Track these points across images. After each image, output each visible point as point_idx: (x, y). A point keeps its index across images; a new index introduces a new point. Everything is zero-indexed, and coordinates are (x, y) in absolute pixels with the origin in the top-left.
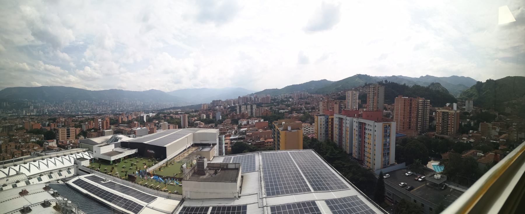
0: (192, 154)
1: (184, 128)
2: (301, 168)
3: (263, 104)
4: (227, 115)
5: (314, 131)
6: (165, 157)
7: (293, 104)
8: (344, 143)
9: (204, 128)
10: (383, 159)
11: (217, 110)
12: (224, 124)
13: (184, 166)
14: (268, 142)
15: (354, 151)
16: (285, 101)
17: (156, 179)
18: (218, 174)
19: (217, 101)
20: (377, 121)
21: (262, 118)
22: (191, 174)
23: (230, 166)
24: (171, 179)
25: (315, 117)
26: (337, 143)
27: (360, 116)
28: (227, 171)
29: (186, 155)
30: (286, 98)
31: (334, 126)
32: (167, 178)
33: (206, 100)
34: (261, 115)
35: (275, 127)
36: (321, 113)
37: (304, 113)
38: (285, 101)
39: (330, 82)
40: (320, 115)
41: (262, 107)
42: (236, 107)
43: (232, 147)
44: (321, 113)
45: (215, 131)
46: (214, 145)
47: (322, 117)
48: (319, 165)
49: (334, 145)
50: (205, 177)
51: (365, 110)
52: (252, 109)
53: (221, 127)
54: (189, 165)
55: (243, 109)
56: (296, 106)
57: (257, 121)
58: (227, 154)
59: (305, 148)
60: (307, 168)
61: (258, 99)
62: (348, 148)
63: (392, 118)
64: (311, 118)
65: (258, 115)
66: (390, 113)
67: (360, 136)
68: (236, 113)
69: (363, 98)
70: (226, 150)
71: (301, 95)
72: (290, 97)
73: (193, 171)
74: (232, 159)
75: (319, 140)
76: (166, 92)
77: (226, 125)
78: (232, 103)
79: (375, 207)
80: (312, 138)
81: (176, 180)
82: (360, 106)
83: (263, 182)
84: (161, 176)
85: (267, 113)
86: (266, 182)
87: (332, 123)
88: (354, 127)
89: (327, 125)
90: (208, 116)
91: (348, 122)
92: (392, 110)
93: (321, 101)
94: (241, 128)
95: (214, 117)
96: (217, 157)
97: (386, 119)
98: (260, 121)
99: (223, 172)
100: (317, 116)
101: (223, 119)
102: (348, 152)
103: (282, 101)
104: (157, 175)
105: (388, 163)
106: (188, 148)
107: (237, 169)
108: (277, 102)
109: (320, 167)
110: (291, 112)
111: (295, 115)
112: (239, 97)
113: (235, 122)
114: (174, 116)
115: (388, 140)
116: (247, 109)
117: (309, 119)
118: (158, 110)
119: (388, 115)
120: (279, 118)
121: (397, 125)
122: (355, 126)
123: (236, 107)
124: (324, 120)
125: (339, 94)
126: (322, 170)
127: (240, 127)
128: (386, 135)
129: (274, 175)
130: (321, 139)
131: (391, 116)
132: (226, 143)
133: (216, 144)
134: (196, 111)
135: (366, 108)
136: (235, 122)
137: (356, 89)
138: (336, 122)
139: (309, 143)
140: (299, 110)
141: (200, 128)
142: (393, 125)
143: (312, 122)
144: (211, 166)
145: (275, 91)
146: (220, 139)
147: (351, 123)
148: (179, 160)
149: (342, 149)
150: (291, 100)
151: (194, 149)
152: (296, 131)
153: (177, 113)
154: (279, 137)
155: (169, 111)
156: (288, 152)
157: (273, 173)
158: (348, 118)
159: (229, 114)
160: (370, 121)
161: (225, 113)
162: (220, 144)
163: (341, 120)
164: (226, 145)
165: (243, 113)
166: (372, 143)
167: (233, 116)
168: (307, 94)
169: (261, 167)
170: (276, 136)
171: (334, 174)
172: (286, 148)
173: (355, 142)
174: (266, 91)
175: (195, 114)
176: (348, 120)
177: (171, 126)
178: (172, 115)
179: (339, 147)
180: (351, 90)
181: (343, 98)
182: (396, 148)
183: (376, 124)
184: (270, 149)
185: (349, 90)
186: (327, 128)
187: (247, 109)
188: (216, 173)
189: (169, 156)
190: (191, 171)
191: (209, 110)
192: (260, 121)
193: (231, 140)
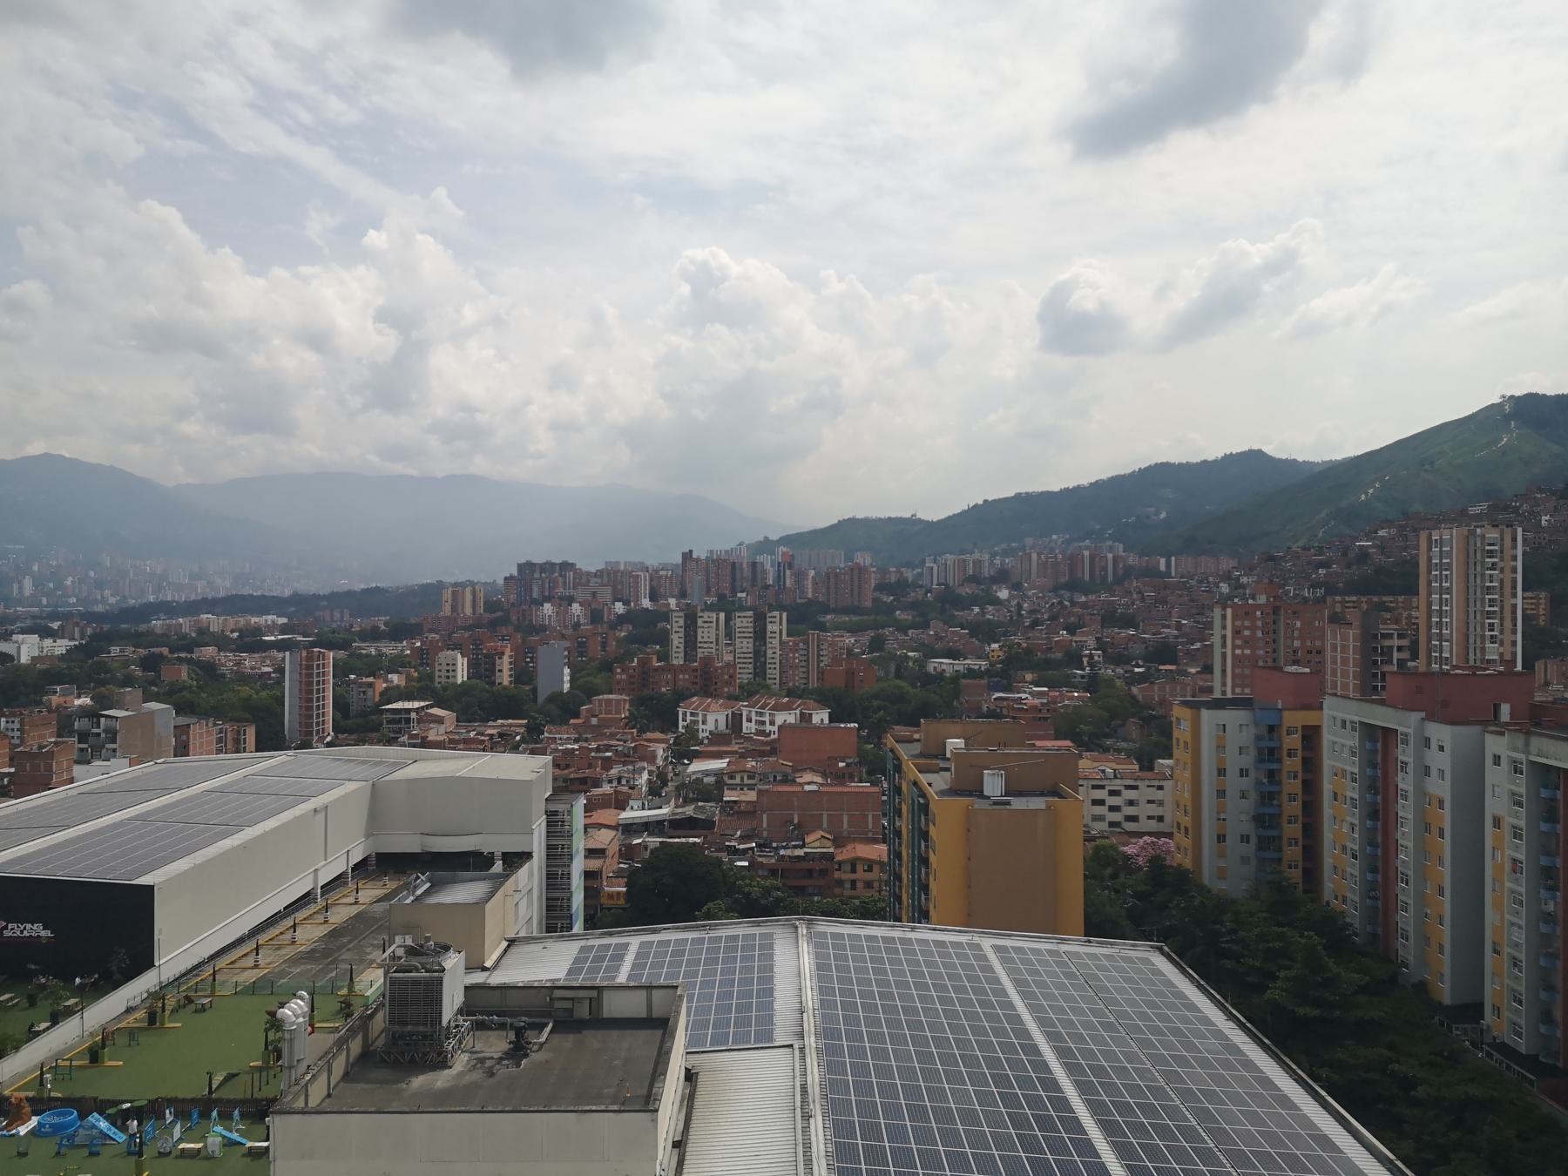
0: (360, 925)
1: (306, 745)
3: (826, 610)
4: (607, 667)
5: (1167, 811)
6: (143, 960)
7: (1016, 622)
8: (1406, 919)
9: (451, 744)
11: (543, 628)
12: (587, 726)
13: (294, 1011)
14: (853, 864)
15: (1491, 990)
16: (964, 603)
17: (57, 1129)
19: (548, 567)
21: (823, 700)
22: (339, 1066)
23: (615, 1006)
24: (179, 1115)
25: (1178, 712)
28: (592, 1038)
29: (310, 934)
30: (975, 579)
31: (1327, 788)
32: (150, 1111)
34: (814, 683)
35: (898, 768)
37: (1092, 684)
38: (964, 603)
39: (1291, 464)
40: (1220, 704)
41: (822, 627)
42: (665, 616)
43: (631, 877)
44: (1223, 684)
45: (526, 768)
46: (515, 860)
47: (1234, 718)
48: (1204, 1063)
49: (1331, 927)
50: (441, 1079)
52: (760, 635)
53: (564, 740)
54: (330, 1005)
55: (709, 630)
56: (1039, 636)
57: (790, 718)
58: (593, 922)
59: (1097, 927)
60: (1121, 1071)
61: (800, 576)
64: (1147, 721)
65: (797, 680)
68: (664, 656)
70: (591, 893)
71: (1074, 561)
72: (1002, 577)
73: (356, 1046)
74: (633, 955)
76: (175, 475)
77: (597, 731)
78: (644, 589)
80: (1157, 864)
81: (225, 1117)
83: (817, 1123)
84: (101, 1107)
85: (850, 674)
86: (840, 1129)
87: (1311, 763)
88: (1495, 804)
90: (483, 667)
91: (1439, 761)
93: (1224, 602)
98: (806, 718)
99: (568, 1041)
100: (1195, 706)
101: (584, 691)
102: (1445, 992)
103: (949, 601)
104: (68, 1102)
106: (328, 887)
107: (662, 1025)
108: (914, 605)
110: (1004, 675)
111: (1030, 695)
113: (656, 712)
114: (227, 661)
116: (729, 634)
117: (1133, 727)
118: (90, 617)
120: (926, 711)
124: (1247, 737)
125: (1364, 555)
126: (1236, 1099)
127: (684, 750)
129: (888, 1090)
130: (1222, 874)
132: (591, 853)
133: (528, 856)
134: (398, 632)
136: (656, 712)
138: (1340, 757)
139: (1134, 899)
141: (425, 744)
143: (1153, 743)
144: (488, 1007)
146: (556, 825)
148: (250, 977)
150: (1003, 594)
151: (370, 893)
152: (1038, 803)
153: (251, 642)
154: (925, 835)
155: (185, 623)
156: (987, 943)
157: (884, 1072)
158: (1440, 733)
159: (623, 659)
161: (596, 650)
162: (557, 855)
163: (1379, 741)
164: (595, 864)
165: (707, 661)
167: (645, 673)
168: (1113, 551)
169: (809, 1024)
170: (904, 825)
171: (1325, 1142)
174: (848, 531)
175: (389, 649)
176: (1435, 750)
177: (202, 732)
178: (209, 652)
180: (1460, 517)
181: (1400, 579)
184: (868, 912)
185: (1438, 521)
187: (729, 634)
188: (518, 1050)
189: (175, 953)
190: (341, 1043)
191: (493, 625)
192: (806, 718)
193: (629, 829)
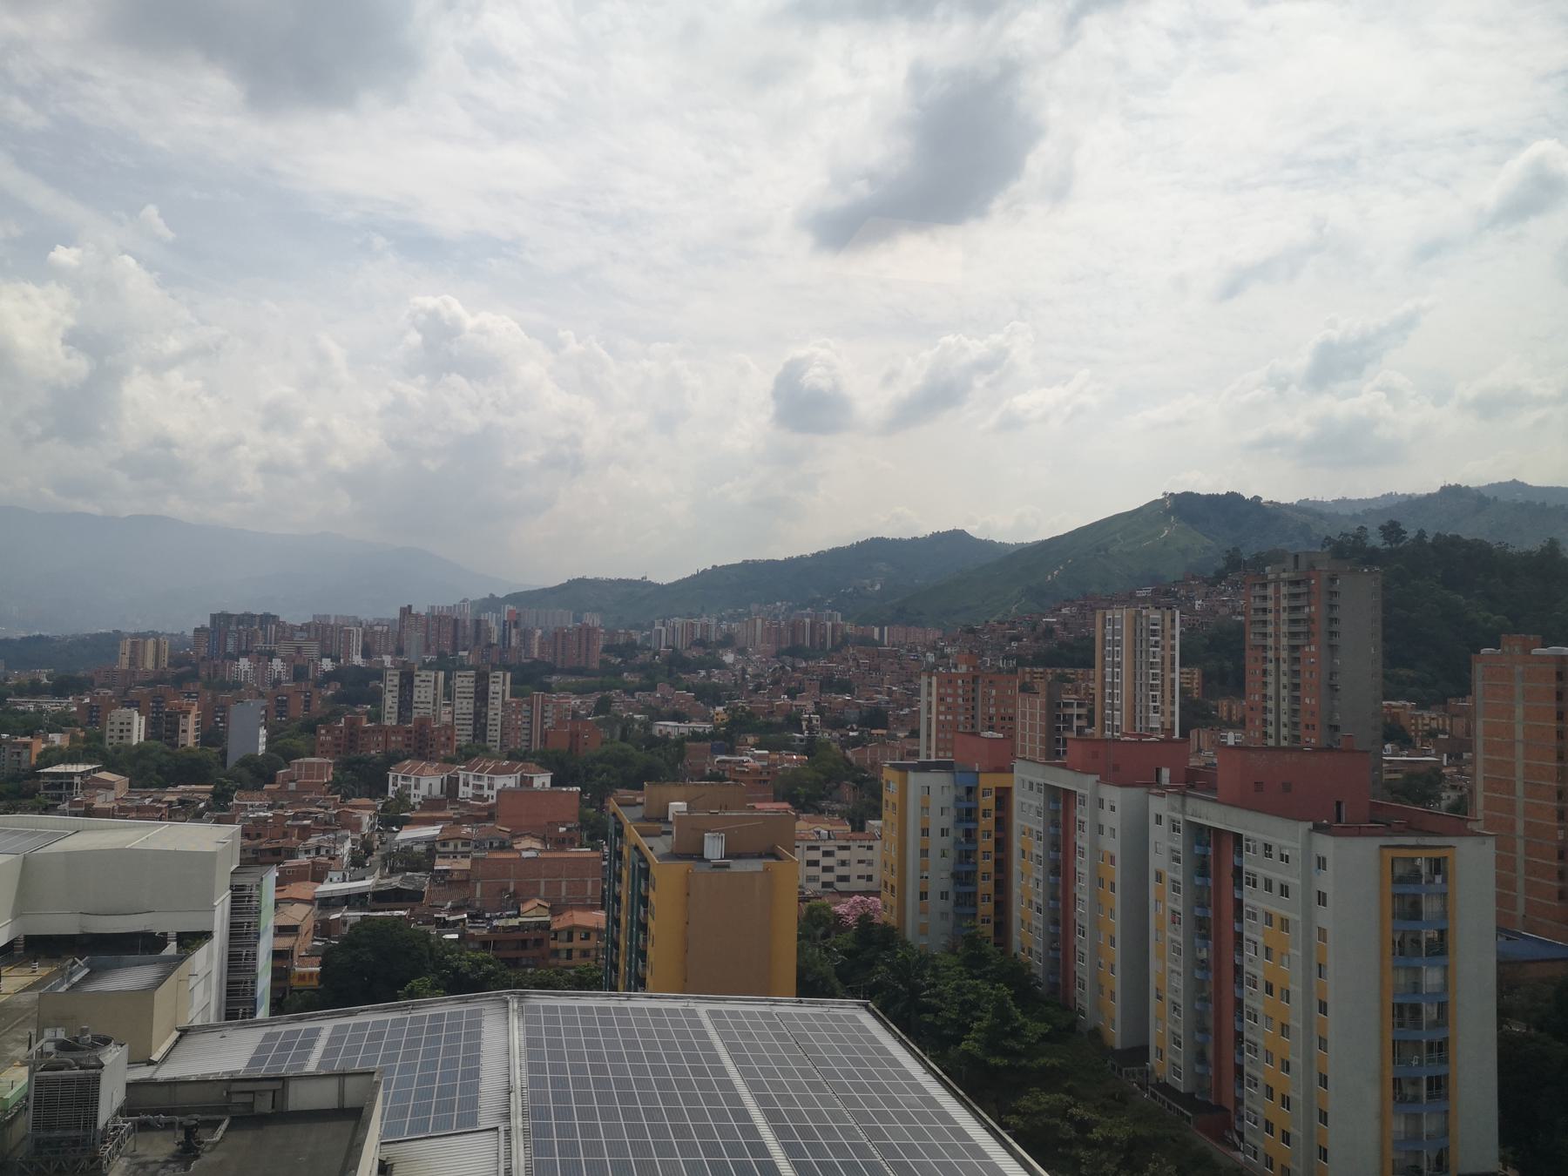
3: (553, 670)
4: (310, 728)
5: (877, 872)
8: (1082, 969)
9: (122, 812)
10: (1399, 1126)
11: (237, 685)
14: (570, 933)
15: (1158, 1034)
16: (689, 666)
18: (207, 1158)
20: (1334, 822)
21: (546, 762)
23: (301, 1097)
25: (889, 776)
26: (1038, 967)
27: (1193, 782)
30: (702, 643)
31: (1016, 846)
34: (536, 746)
35: (620, 832)
36: (928, 750)
37: (810, 748)
38: (689, 666)
39: (989, 545)
40: (924, 767)
41: (547, 688)
42: (379, 675)
46: (192, 940)
47: (937, 781)
48: (904, 1118)
49: (1017, 977)
51: (1231, 738)
52: (482, 696)
53: (256, 806)
55: (426, 690)
57: (510, 782)
59: (809, 986)
61: (526, 636)
62: (1116, 1008)
63: (1461, 807)
64: (860, 783)
65: (521, 745)
66: (1436, 770)
67: (1203, 928)
68: (376, 717)
69: (1219, 660)
71: (795, 628)
72: (728, 641)
74: (323, 1040)
75: (910, 934)
78: (357, 643)
79: (943, 1091)
80: (865, 921)
82: (1195, 715)
85: (575, 736)
87: (1003, 823)
88: (1158, 861)
89: (969, 834)
90: (164, 726)
91: (1112, 820)
92: (1458, 749)
93: (931, 670)
94: (403, 823)
95: (212, 736)
96: (205, 1029)
97: (1408, 808)
98: (526, 782)
99: (245, 1138)
100: (903, 769)
101: (282, 753)
102: (1116, 1036)
103: (677, 664)
107: (353, 1116)
108: (642, 668)
110: (727, 739)
111: (752, 757)
112: (406, 611)
113: (364, 775)
115: (1431, 978)
116: (449, 694)
117: (847, 789)
119: (1420, 787)
120: (649, 774)
123: (379, 675)
125: (1049, 631)
127: (392, 818)
128: (1415, 932)
130: (923, 930)
131: (1448, 797)
132: (281, 931)
133: (206, 935)
134: (61, 688)
135: (1241, 724)
136: (364, 775)
137: (1165, 596)
139: (847, 959)
140: (779, 728)
141: (90, 812)
142: (1474, 865)
143: (865, 807)
144: (153, 1106)
146: (242, 901)
150: (729, 658)
152: (756, 865)
154: (644, 901)
156: (702, 1009)
159: (325, 720)
160: (1276, 823)
161: (298, 711)
162: (241, 935)
163: (1061, 802)
164: (285, 943)
165: (423, 723)
166: (1296, 989)
167: (353, 735)
170: (624, 891)
172: (692, 982)
173: (1169, 972)
174: (578, 592)
175: (51, 705)
176: (1109, 808)
179: (1046, 998)
180: (1129, 599)
181: (1073, 654)
182: (1507, 1045)
183: (1326, 845)
184: (584, 983)
185: (1112, 601)
186: (966, 856)
187: (449, 694)
188: (188, 1151)
191: (179, 681)
192: (526, 782)
193: (327, 903)
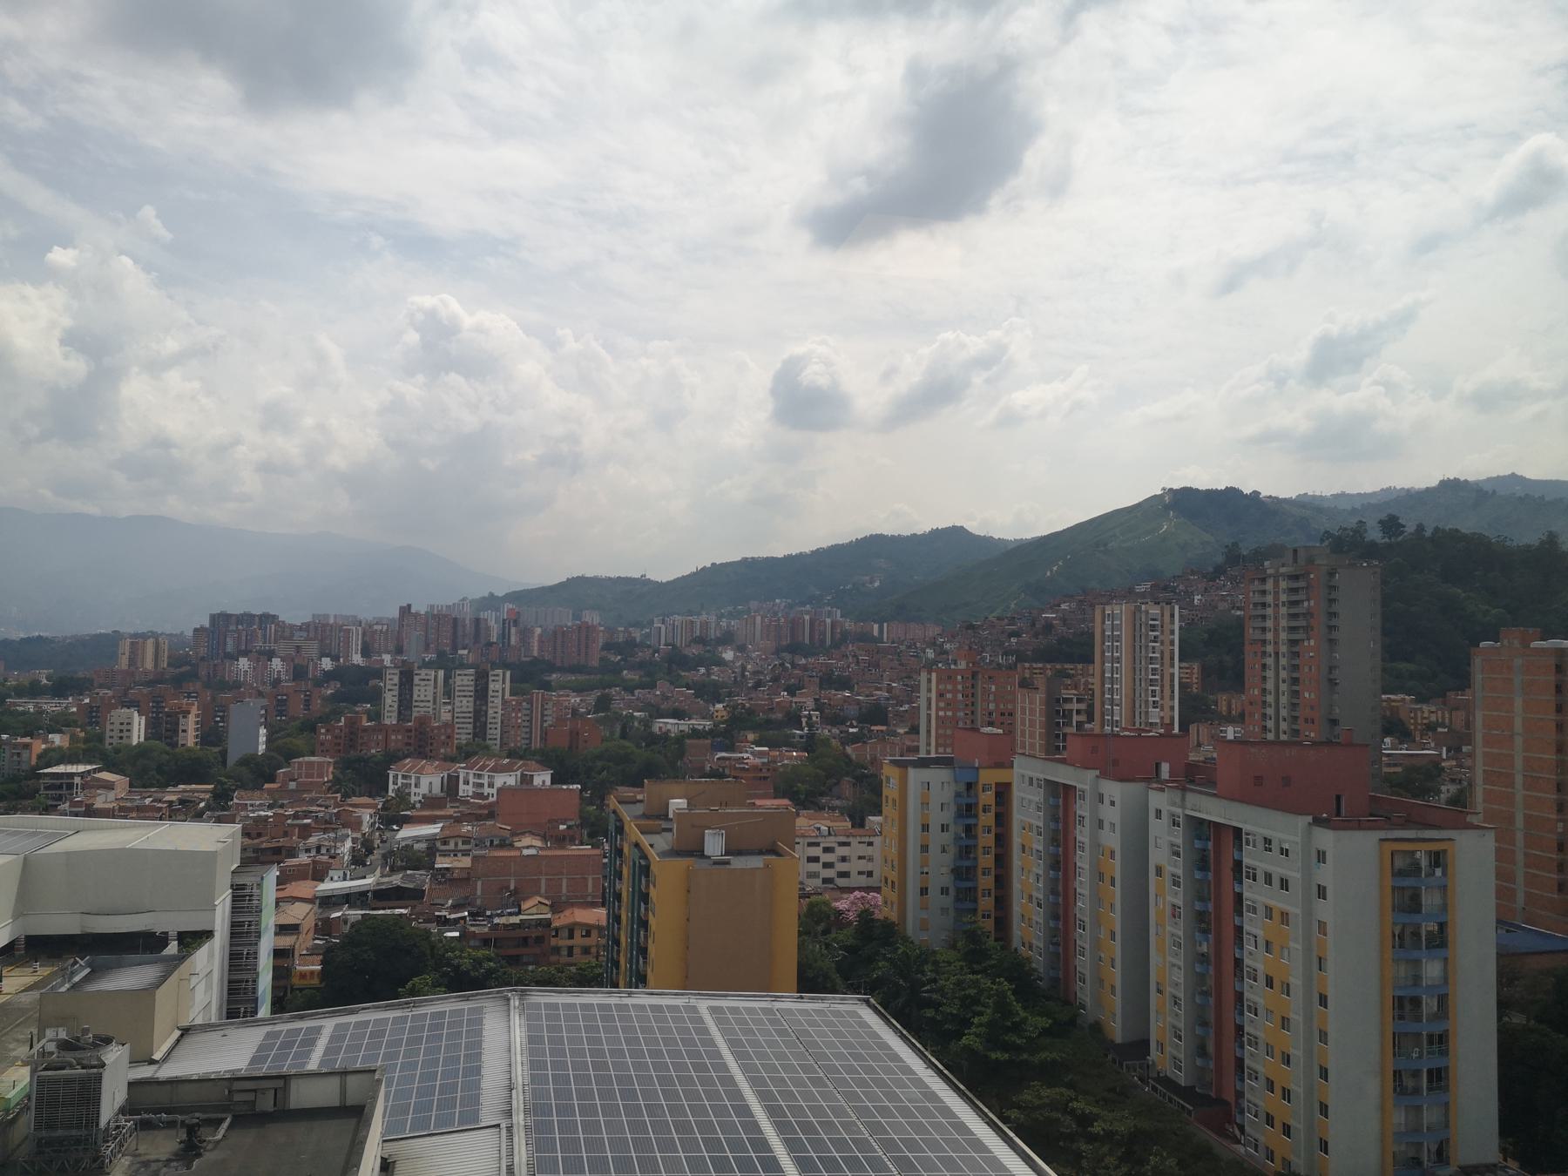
2: (782, 1127)
3: (552, 668)
4: (310, 727)
8: (1083, 964)
9: (122, 812)
10: (1399, 1118)
11: (237, 685)
14: (571, 930)
15: (1158, 1028)
18: (209, 1156)
19: (246, 619)
20: (1334, 815)
21: (546, 760)
23: (304, 1095)
25: (890, 773)
26: (1039, 962)
27: (1193, 777)
28: (278, 1134)
30: (701, 640)
31: (1017, 840)
33: (163, 603)
34: (537, 744)
35: (620, 829)
36: (928, 746)
37: (810, 744)
39: (987, 541)
40: (924, 763)
41: (547, 686)
42: (379, 673)
43: (328, 956)
46: (193, 939)
47: (938, 776)
48: (905, 1112)
49: (1018, 972)
51: (1230, 732)
52: (481, 694)
53: (257, 806)
55: (425, 690)
57: (510, 780)
59: (810, 982)
61: (525, 634)
63: (1460, 801)
64: (860, 779)
67: (1203, 922)
68: (376, 716)
69: (1219, 655)
70: (281, 973)
71: (795, 625)
72: (727, 639)
74: (325, 1039)
77: (295, 797)
78: (356, 643)
80: (866, 917)
82: (1195, 709)
85: (574, 734)
88: (1158, 856)
89: (969, 829)
90: (164, 727)
91: (1111, 815)
92: (1458, 742)
93: (930, 666)
94: (404, 821)
95: (212, 735)
96: (206, 1028)
97: (1406, 801)
98: (526, 780)
99: (247, 1137)
100: (902, 765)
101: (282, 753)
102: (1117, 1031)
103: (676, 662)
105: (1441, 1155)
107: (355, 1114)
108: (642, 665)
109: (919, 1128)
110: (726, 736)
111: (752, 754)
112: (406, 610)
113: (364, 774)
115: (1432, 970)
116: (449, 693)
117: (846, 786)
119: (1420, 780)
120: (650, 772)
121: (1503, 856)
122: (1165, 846)
123: (379, 673)
125: (1049, 626)
127: (392, 817)
128: (1415, 926)
130: (924, 926)
131: (1448, 790)
132: (282, 929)
133: (208, 935)
134: (60, 688)
135: (1240, 719)
136: (364, 774)
137: (1163, 591)
139: (849, 956)
141: (90, 812)
142: (1473, 857)
143: (865, 802)
144: (155, 1105)
145: (633, 593)
146: (242, 899)
147: (1131, 826)
149: (1068, 1001)
150: (729, 655)
152: (756, 862)
154: (645, 898)
156: (703, 1005)
161: (298, 709)
162: (242, 934)
163: (1061, 797)
164: (286, 941)
165: (423, 721)
166: (1296, 982)
167: (353, 734)
168: (833, 617)
170: (624, 888)
172: (692, 979)
173: (1169, 966)
174: (577, 590)
175: (51, 706)
176: (1108, 804)
179: (1047, 993)
180: (1129, 594)
181: (1073, 650)
183: (1325, 838)
184: (586, 980)
185: (1112, 597)
186: (966, 851)
187: (449, 693)
188: (190, 1150)
191: (178, 681)
192: (526, 780)
193: (328, 901)
